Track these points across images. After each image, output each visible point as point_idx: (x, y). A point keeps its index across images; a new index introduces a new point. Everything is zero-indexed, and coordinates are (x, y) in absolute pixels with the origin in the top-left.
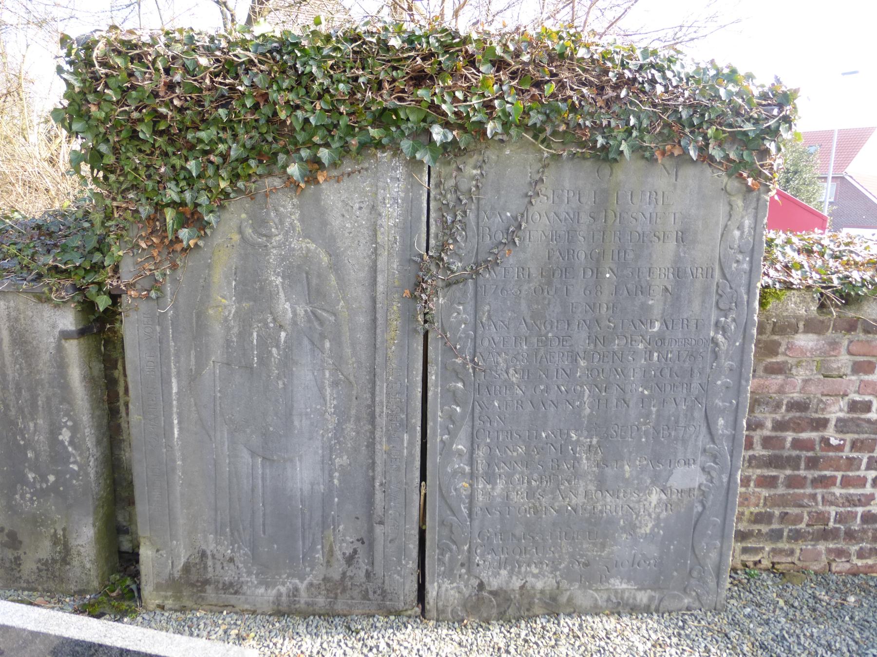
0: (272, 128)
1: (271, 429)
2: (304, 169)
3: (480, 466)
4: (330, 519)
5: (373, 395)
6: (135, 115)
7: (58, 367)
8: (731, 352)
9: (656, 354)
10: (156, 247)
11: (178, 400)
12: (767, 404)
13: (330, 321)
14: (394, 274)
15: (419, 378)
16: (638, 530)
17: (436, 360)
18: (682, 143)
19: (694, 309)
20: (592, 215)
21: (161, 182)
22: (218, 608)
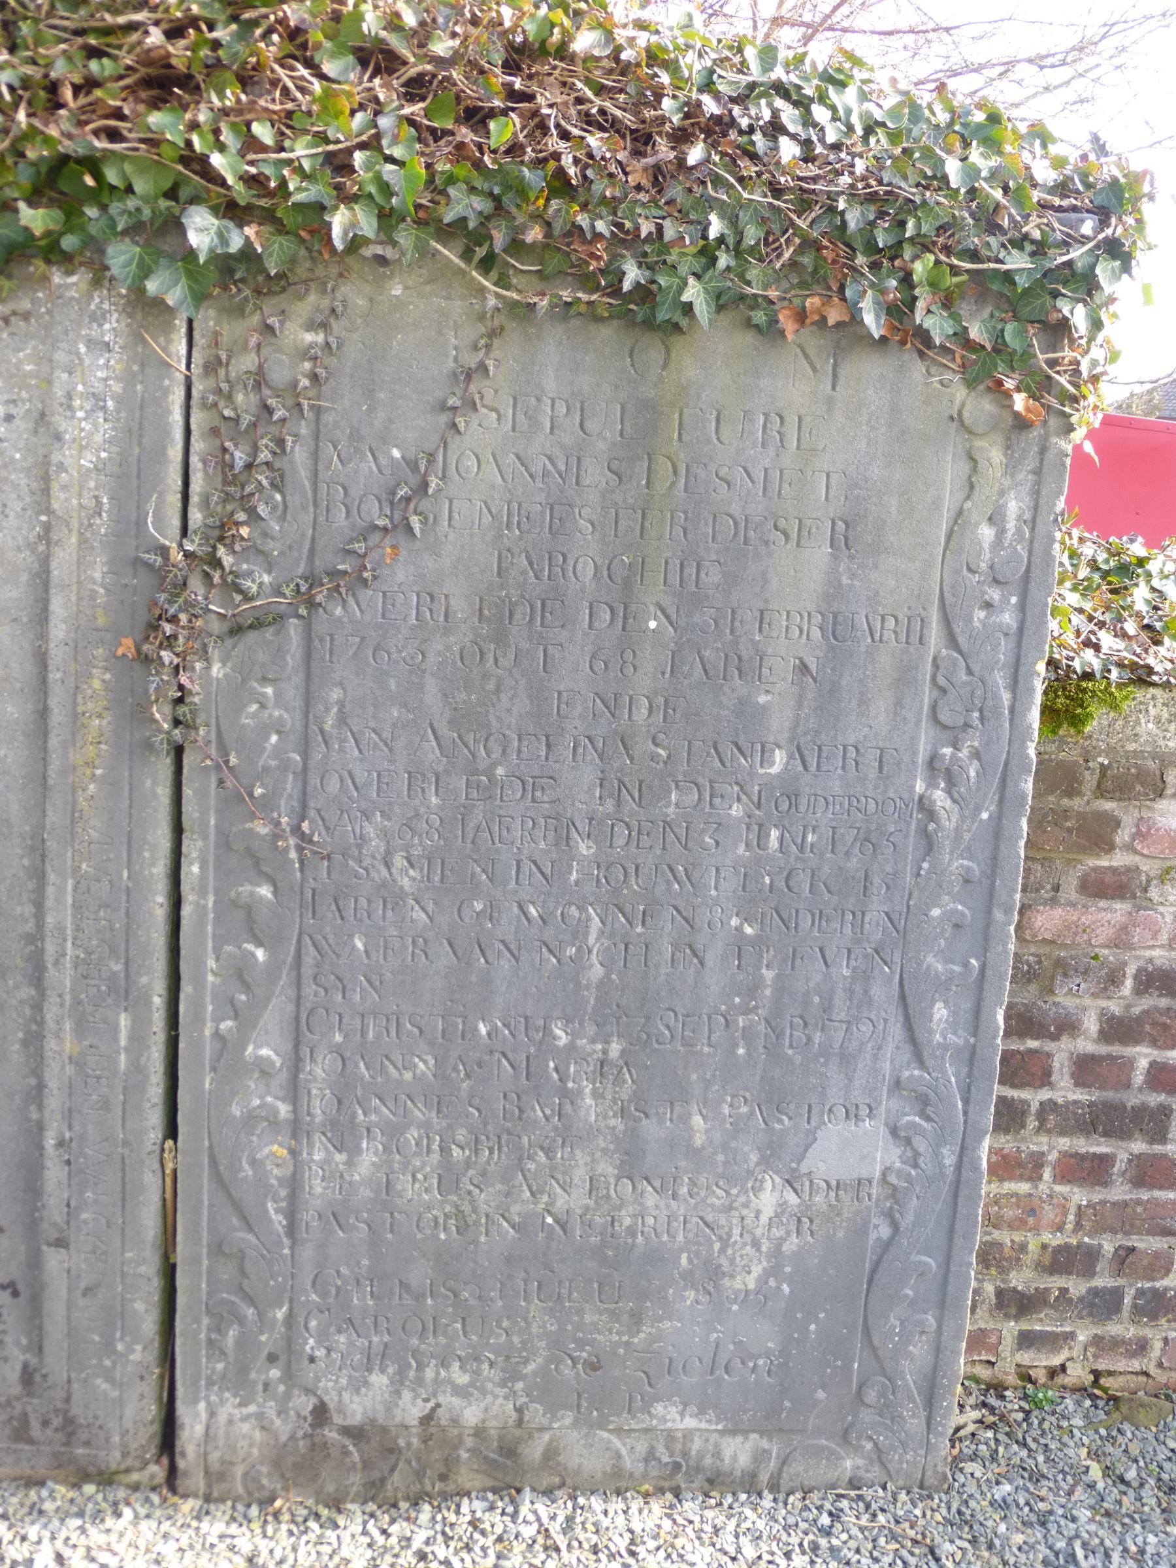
3: (316, 1103)
8: (967, 837)
9: (774, 834)
12: (1085, 973)
14: (93, 595)
15: (160, 869)
16: (726, 1282)
17: (204, 824)
18: (848, 293)
19: (873, 721)
20: (615, 465)
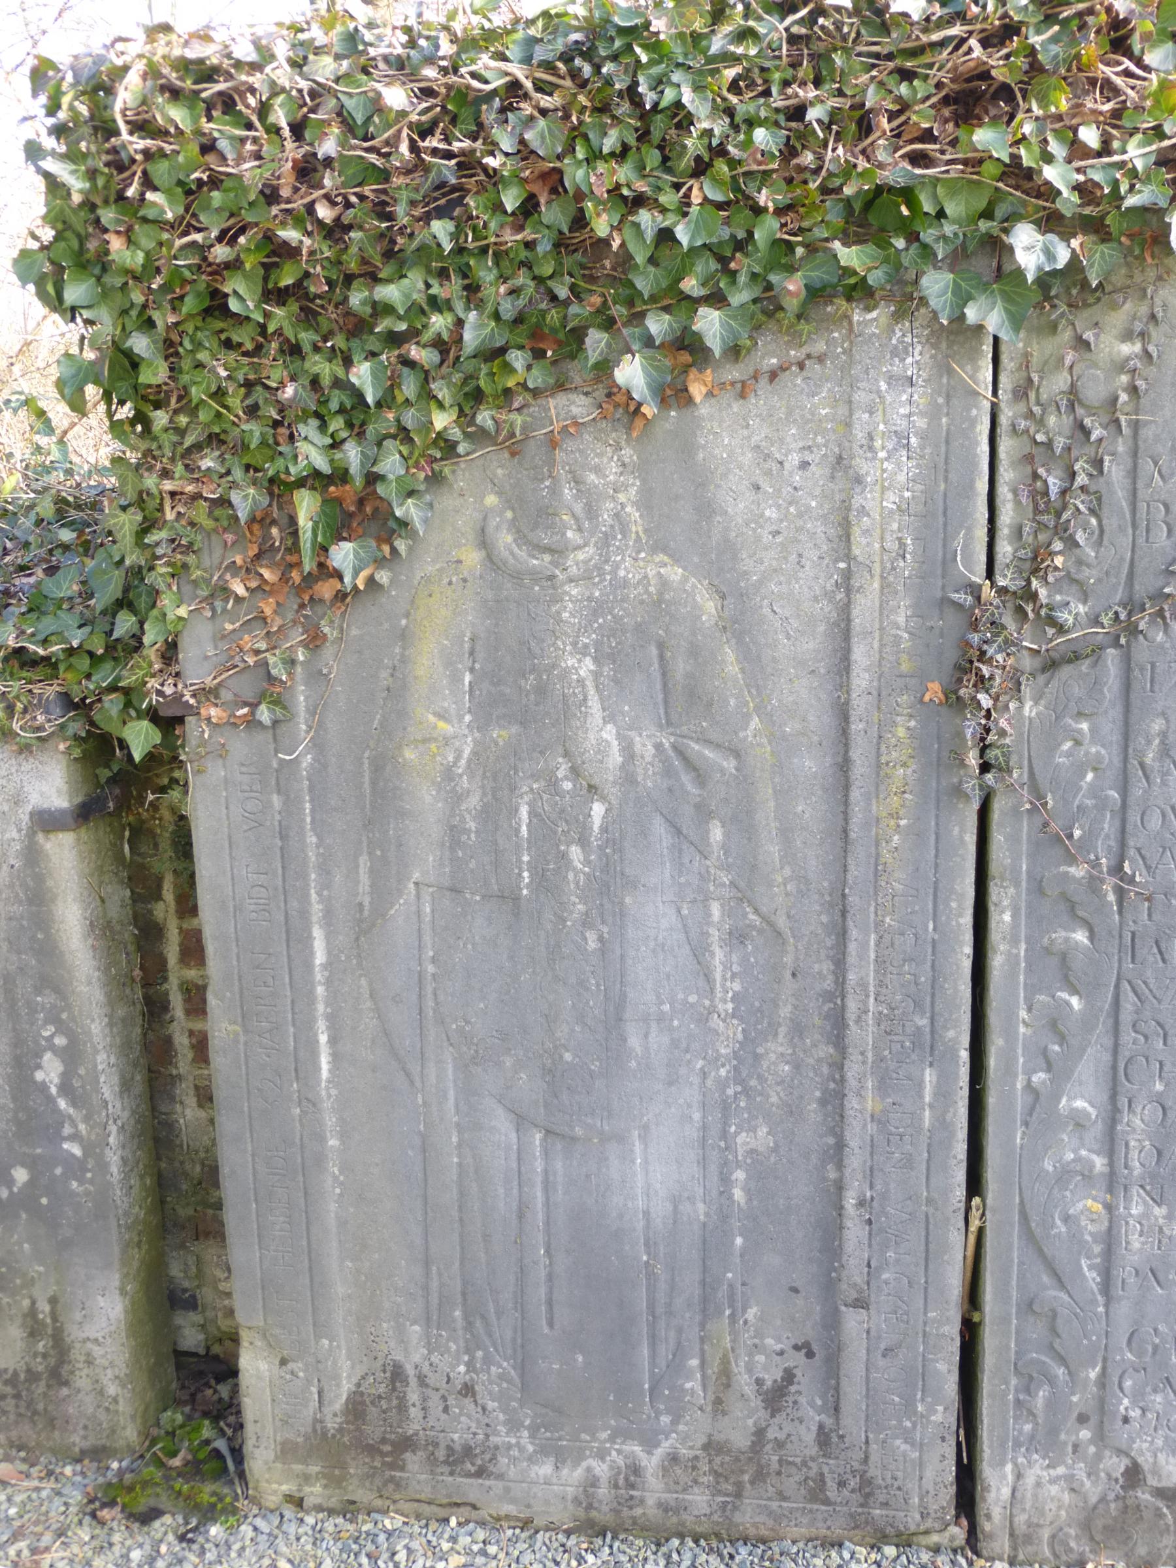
0: (568, 261)
1: (568, 1057)
2: (656, 368)
3: (1134, 1155)
4: (722, 1293)
5: (840, 964)
6: (221, 253)
7: (30, 901)
10: (271, 593)
11: (328, 982)
13: (723, 771)
15: (967, 920)
17: (1015, 870)
21: (283, 424)
22: (438, 1511)
